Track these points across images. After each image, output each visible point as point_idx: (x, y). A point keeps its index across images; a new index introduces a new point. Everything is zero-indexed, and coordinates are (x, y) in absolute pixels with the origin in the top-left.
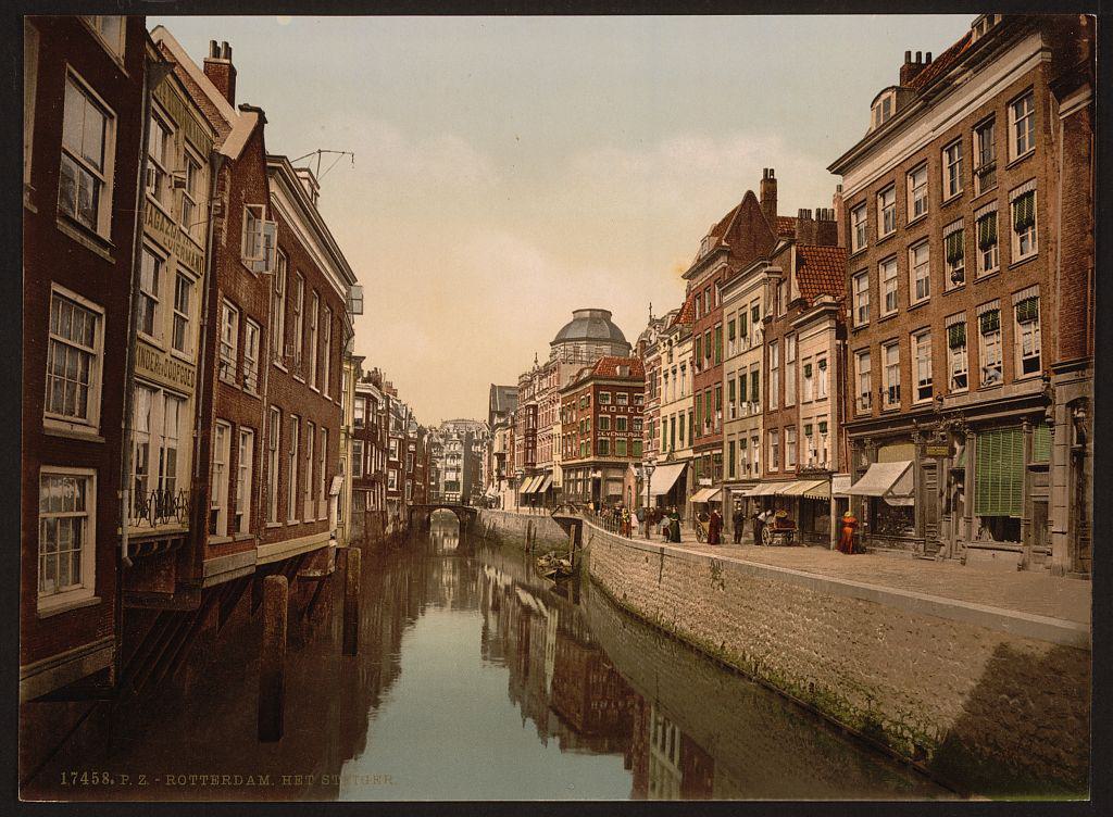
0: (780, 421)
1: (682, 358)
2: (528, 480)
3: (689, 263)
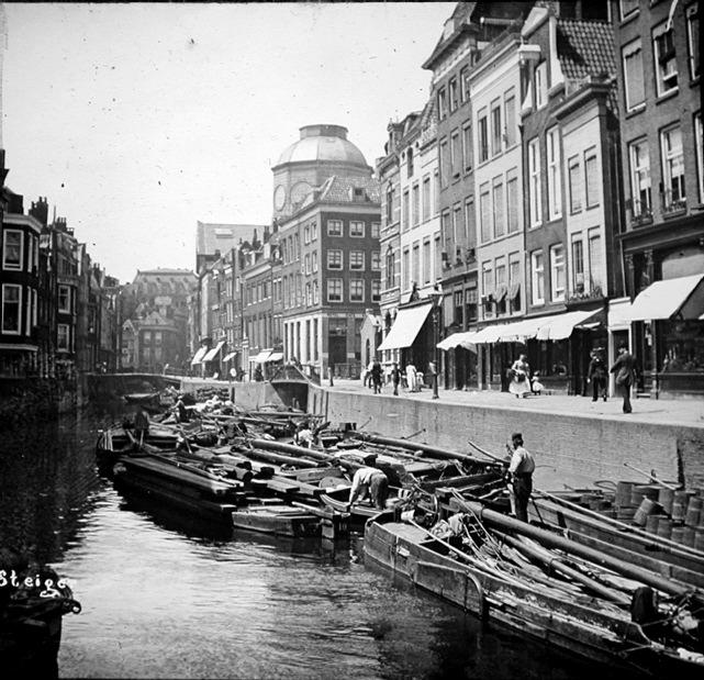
0: (548, 239)
1: (425, 171)
3: (427, 53)
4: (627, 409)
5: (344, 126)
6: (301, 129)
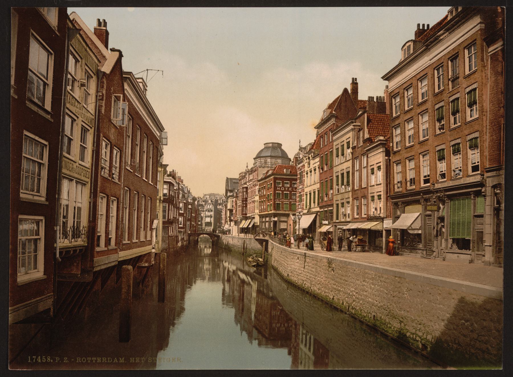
1: (315, 165)
2: (244, 222)
3: (317, 121)
4: (398, 173)
6: (264, 144)
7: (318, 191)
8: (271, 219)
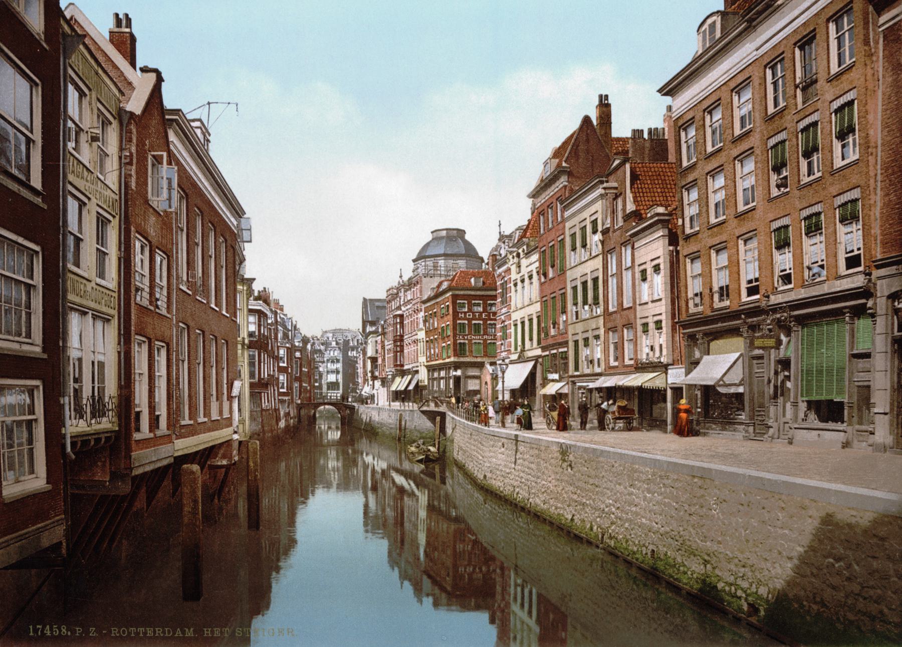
0: (619, 321)
1: (529, 269)
5: (462, 228)
7: (538, 317)
8: (449, 372)
